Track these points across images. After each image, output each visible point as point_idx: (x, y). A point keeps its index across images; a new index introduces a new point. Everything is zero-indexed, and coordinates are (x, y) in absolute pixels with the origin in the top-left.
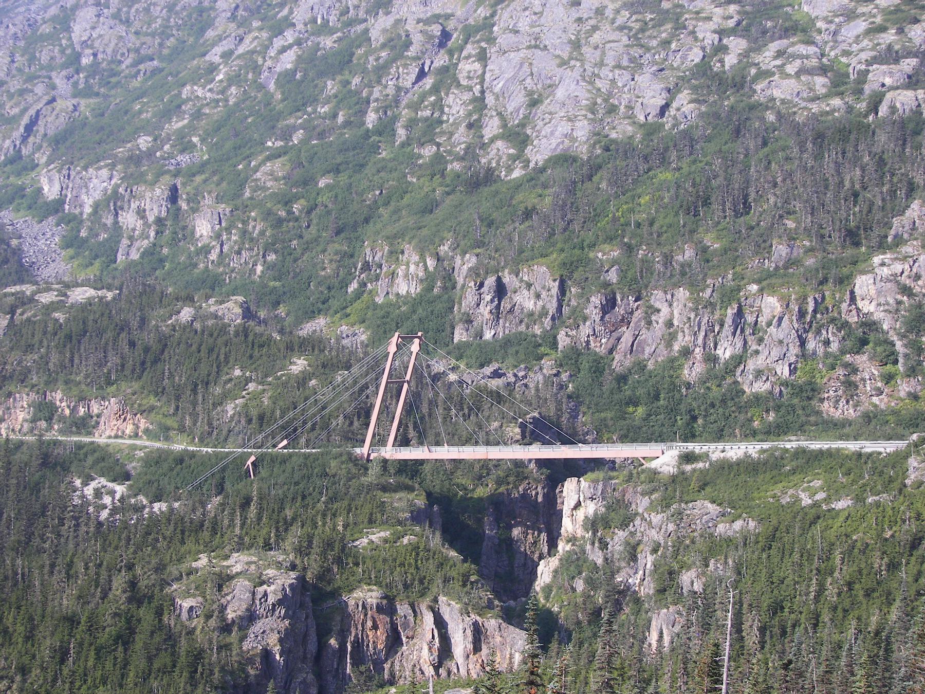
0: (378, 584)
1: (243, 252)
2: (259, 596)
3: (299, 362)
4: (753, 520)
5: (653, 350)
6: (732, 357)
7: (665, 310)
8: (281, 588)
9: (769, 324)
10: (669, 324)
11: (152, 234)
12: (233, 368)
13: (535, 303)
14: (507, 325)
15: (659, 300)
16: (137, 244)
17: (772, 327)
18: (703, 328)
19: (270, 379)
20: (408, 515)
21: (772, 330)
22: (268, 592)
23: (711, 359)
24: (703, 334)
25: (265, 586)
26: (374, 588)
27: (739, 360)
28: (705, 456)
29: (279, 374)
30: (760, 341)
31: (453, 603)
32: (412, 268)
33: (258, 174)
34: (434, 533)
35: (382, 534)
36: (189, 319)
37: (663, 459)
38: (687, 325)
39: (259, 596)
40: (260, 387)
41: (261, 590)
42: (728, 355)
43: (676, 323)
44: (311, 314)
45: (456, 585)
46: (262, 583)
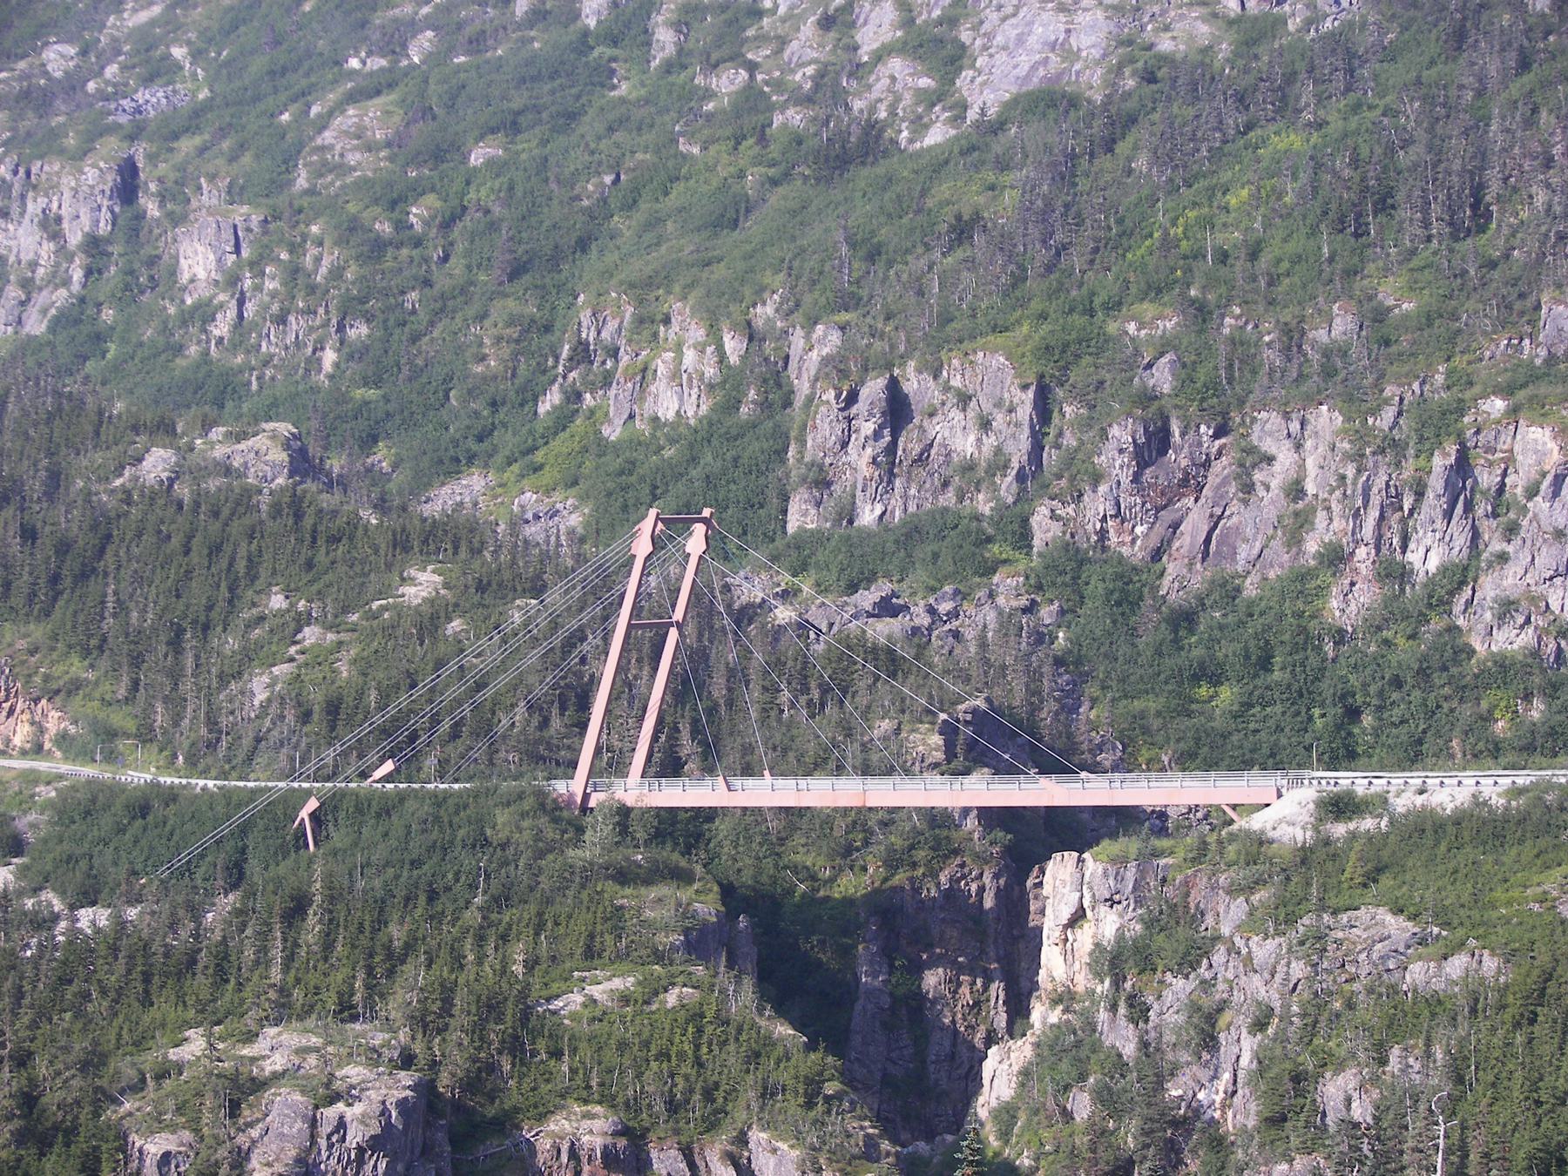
0: (608, 1100)
1: (292, 318)
2: (325, 1129)
3: (423, 577)
4: (1493, 954)
5: (1256, 551)
6: (1444, 570)
7: (1285, 457)
8: (377, 1109)
9: (1532, 492)
10: (1296, 490)
11: (77, 275)
12: (265, 592)
13: (979, 440)
14: (913, 491)
15: (1270, 434)
16: (41, 299)
17: (1538, 499)
18: (1375, 500)
19: (354, 618)
20: (677, 938)
21: (1540, 504)
22: (348, 1119)
23: (1394, 573)
24: (1373, 514)
25: (340, 1106)
26: (598, 1109)
27: (1460, 576)
28: (1379, 803)
29: (375, 605)
30: (1511, 531)
31: (783, 1146)
32: (690, 357)
33: (327, 134)
34: (738, 981)
35: (617, 983)
36: (164, 475)
37: (1279, 810)
38: (1338, 493)
39: (325, 1129)
40: (331, 637)
41: (331, 1113)
42: (1433, 564)
43: (1310, 488)
44: (452, 466)
45: (792, 1105)
46: (333, 1099)
